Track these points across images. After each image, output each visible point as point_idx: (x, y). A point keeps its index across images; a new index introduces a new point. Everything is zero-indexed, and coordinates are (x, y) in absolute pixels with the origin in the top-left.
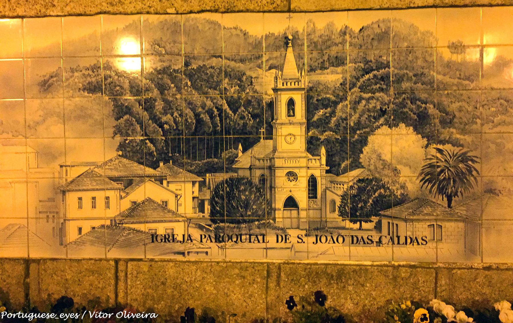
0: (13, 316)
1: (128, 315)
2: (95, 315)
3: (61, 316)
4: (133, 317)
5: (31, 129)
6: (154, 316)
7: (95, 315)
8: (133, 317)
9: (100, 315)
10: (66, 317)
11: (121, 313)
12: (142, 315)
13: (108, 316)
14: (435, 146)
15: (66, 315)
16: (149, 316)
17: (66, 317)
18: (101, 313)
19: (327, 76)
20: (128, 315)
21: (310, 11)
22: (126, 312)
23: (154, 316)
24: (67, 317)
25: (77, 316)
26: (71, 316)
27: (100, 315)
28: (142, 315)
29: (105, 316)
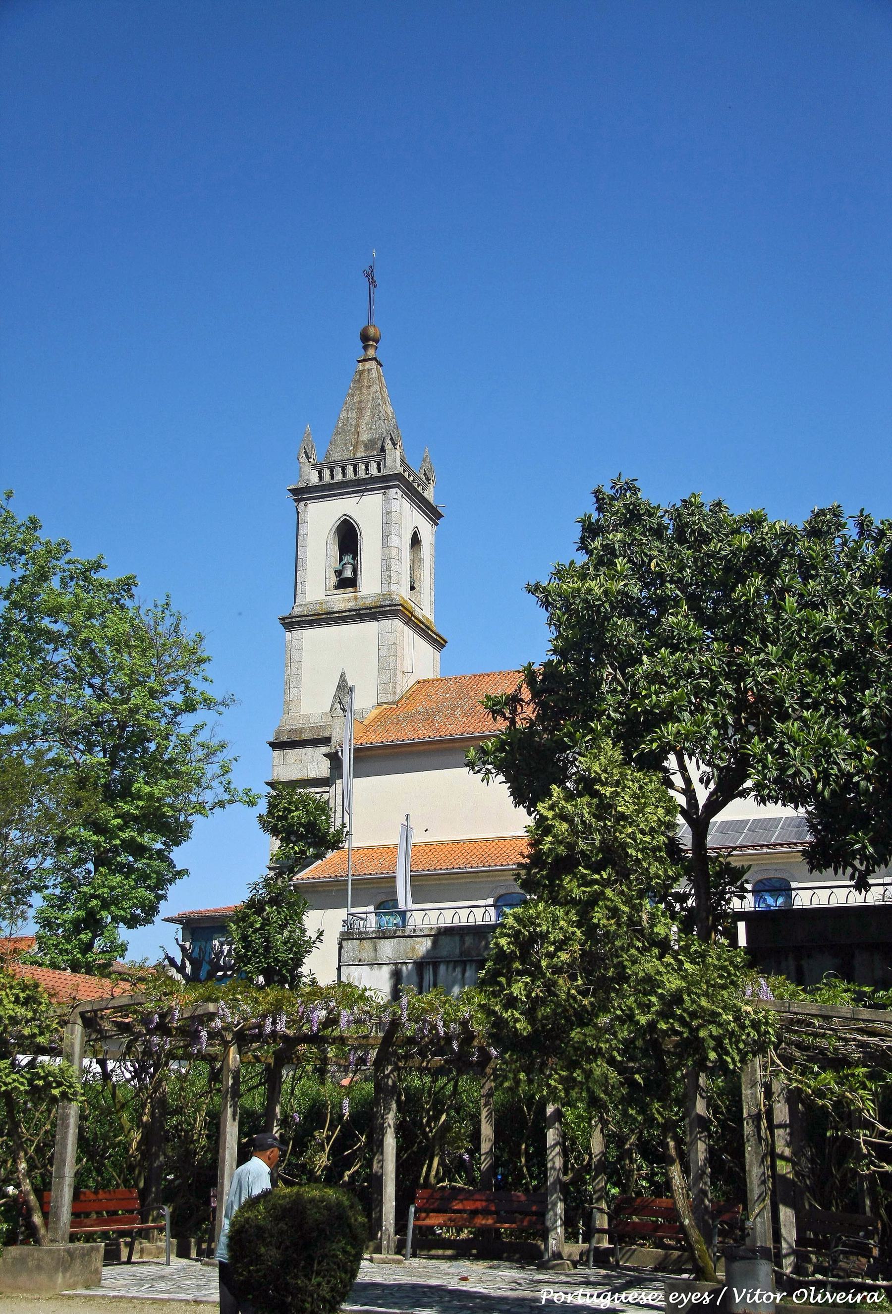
0: (775, 1298)
1: (820, 1296)
2: (745, 1298)
3: (671, 1298)
4: (830, 1301)
5: (247, 792)
6: (875, 1298)
7: (745, 1298)
8: (830, 1301)
9: (756, 1297)
10: (682, 1301)
11: (802, 1293)
12: (850, 1296)
13: (775, 1298)
14: (578, 1030)
15: (683, 1295)
16: (865, 1298)
17: (682, 1301)
18: (758, 1292)
19: (176, 730)
20: (820, 1296)
21: (306, 736)
22: (813, 1289)
23: (875, 1298)
24: (686, 1301)
25: (708, 1300)
26: (838, 1298)
27: (756, 1297)
28: (850, 1296)
29: (768, 1298)
